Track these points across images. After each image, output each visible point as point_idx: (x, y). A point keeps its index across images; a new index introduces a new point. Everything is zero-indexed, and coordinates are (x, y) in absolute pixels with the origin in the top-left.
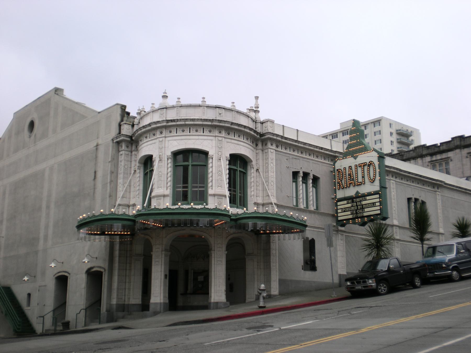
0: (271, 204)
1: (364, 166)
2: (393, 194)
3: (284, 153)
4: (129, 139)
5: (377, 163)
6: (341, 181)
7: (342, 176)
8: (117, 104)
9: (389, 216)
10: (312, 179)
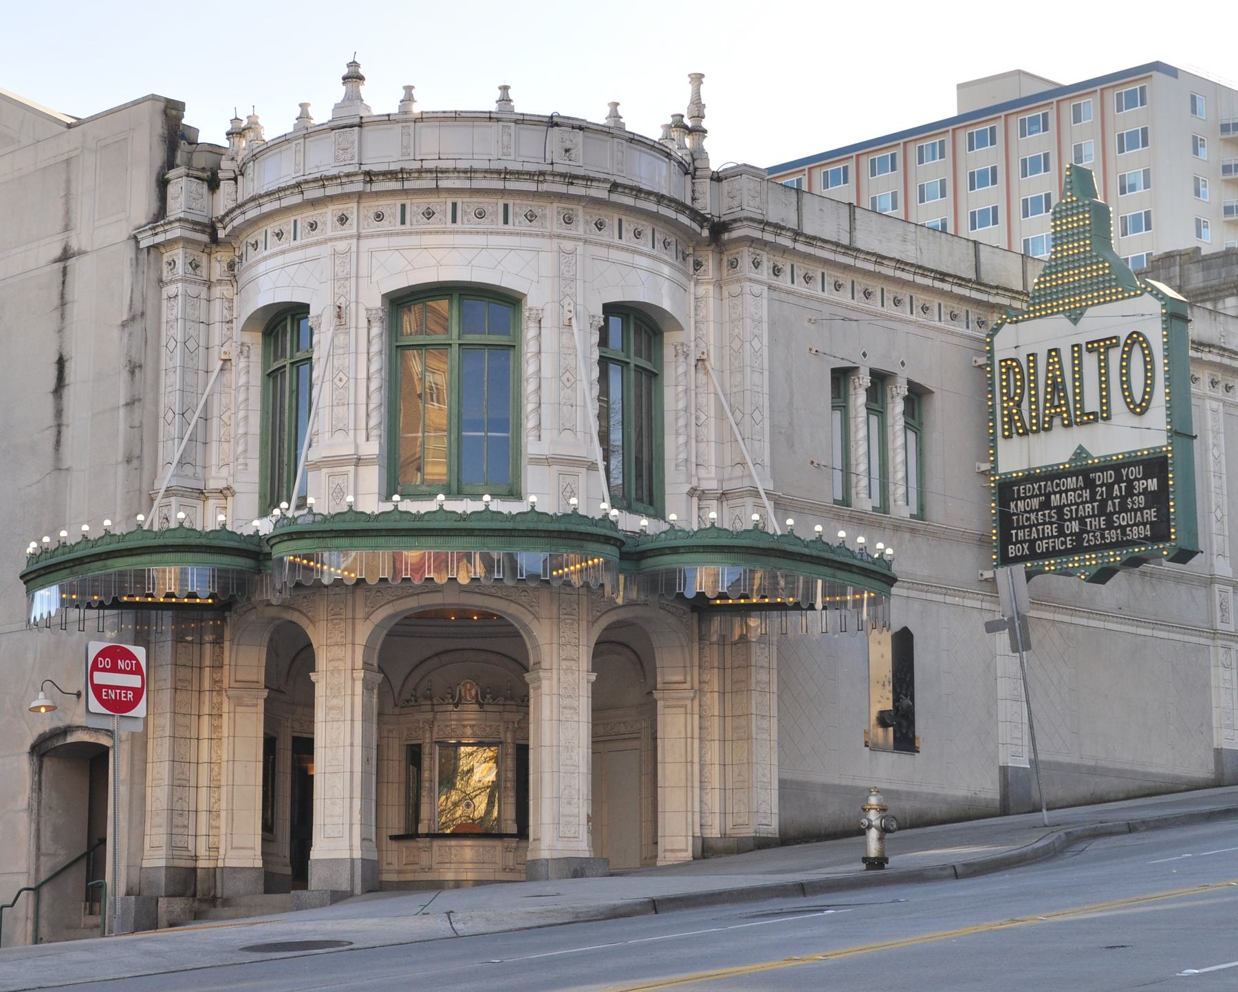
0: (755, 493)
1: (1107, 348)
2: (1213, 453)
3: (800, 296)
4: (205, 238)
5: (1156, 336)
6: (1018, 405)
7: (1022, 380)
8: (153, 98)
9: (1201, 547)
10: (906, 399)
